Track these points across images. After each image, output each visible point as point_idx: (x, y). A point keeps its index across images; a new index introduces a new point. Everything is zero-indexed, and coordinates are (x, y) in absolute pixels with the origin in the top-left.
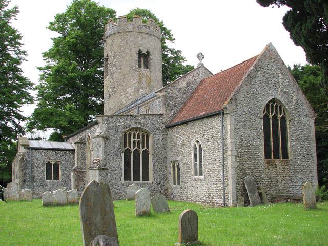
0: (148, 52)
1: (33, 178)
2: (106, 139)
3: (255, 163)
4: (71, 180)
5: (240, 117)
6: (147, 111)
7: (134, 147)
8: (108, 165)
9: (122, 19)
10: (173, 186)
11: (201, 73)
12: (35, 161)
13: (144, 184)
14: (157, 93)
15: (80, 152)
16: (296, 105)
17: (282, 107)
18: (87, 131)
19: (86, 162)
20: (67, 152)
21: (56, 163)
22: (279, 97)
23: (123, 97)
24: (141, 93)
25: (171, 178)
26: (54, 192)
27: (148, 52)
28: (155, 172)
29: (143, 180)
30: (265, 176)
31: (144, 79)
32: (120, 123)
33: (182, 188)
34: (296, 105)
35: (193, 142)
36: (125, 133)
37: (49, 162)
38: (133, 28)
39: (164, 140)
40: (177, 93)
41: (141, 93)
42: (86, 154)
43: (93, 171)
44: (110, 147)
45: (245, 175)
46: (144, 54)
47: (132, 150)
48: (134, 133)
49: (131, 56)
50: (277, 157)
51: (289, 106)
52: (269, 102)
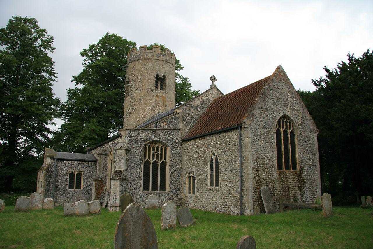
0: (164, 76)
1: (56, 186)
2: (128, 151)
3: (270, 174)
4: (92, 189)
5: (257, 131)
6: (165, 126)
7: (153, 159)
8: (129, 175)
9: (143, 49)
10: (188, 195)
11: (214, 93)
12: (60, 171)
13: (162, 194)
14: (175, 110)
15: (102, 163)
16: (302, 121)
17: (291, 123)
18: (110, 143)
19: (107, 173)
20: (90, 163)
21: (79, 173)
22: (288, 113)
23: (141, 114)
24: (157, 112)
25: (186, 187)
26: (77, 203)
27: (164, 76)
28: (171, 183)
29: (160, 190)
30: (278, 186)
31: (160, 99)
32: (142, 136)
33: (197, 197)
34: (302, 121)
35: (210, 155)
36: (145, 145)
37: (72, 172)
38: (153, 56)
39: (181, 152)
40: (193, 110)
41: (157, 112)
42: (108, 165)
43: (115, 181)
44: (131, 159)
45: (260, 185)
46: (161, 78)
47: (151, 161)
48: (154, 146)
49: (150, 79)
50: (287, 168)
51: (298, 122)
52: (280, 118)
